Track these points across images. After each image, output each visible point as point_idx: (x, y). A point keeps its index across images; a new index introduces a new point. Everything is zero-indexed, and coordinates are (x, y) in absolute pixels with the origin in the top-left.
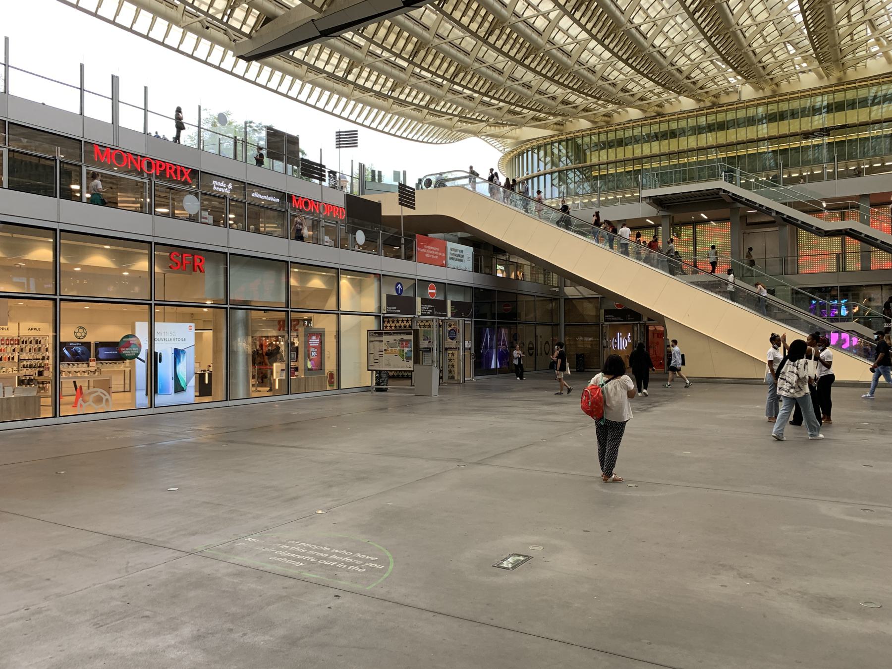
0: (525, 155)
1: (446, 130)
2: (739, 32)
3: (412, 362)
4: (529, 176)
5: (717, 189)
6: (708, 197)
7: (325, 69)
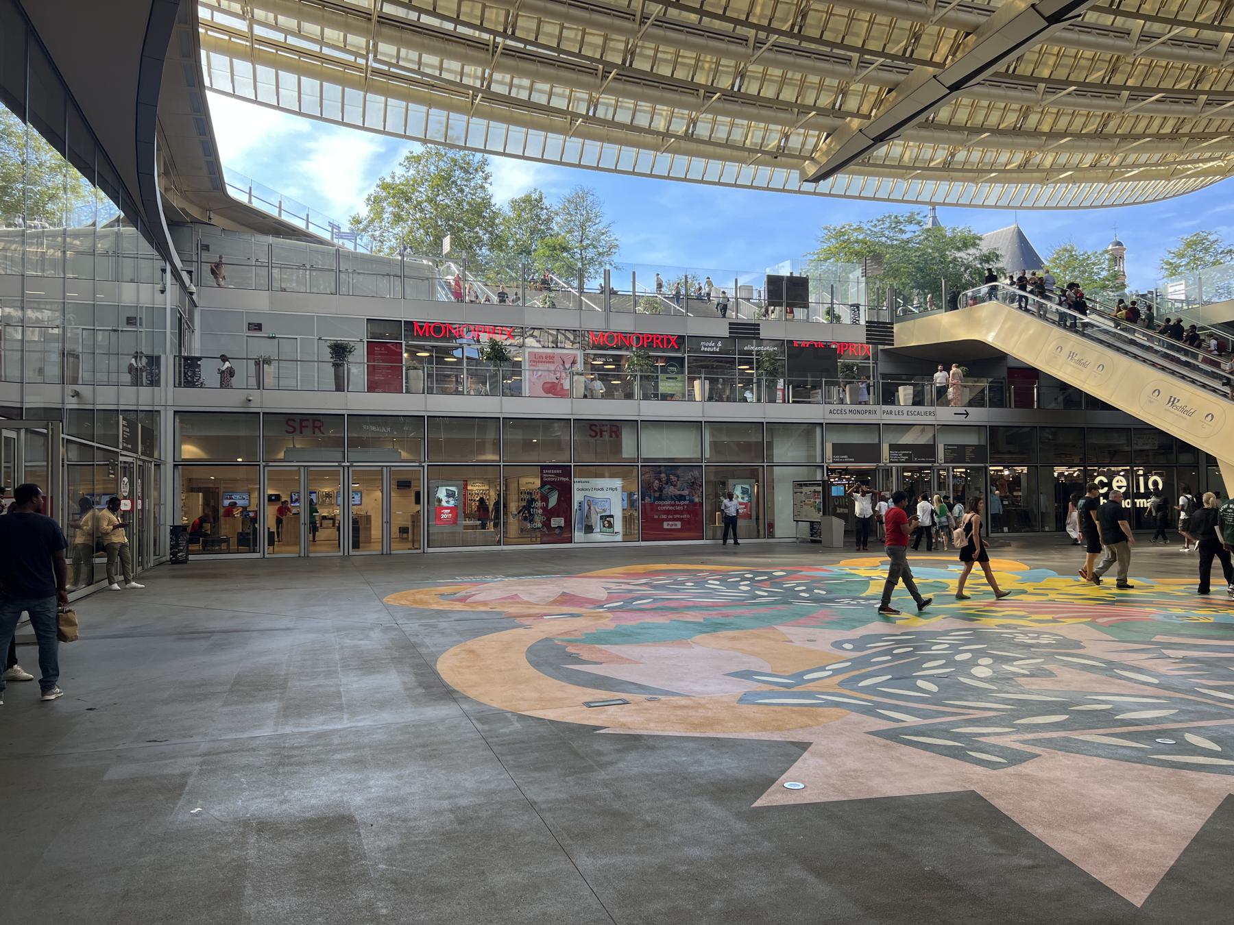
1: (1131, 183)
3: (821, 513)
7: (616, 119)
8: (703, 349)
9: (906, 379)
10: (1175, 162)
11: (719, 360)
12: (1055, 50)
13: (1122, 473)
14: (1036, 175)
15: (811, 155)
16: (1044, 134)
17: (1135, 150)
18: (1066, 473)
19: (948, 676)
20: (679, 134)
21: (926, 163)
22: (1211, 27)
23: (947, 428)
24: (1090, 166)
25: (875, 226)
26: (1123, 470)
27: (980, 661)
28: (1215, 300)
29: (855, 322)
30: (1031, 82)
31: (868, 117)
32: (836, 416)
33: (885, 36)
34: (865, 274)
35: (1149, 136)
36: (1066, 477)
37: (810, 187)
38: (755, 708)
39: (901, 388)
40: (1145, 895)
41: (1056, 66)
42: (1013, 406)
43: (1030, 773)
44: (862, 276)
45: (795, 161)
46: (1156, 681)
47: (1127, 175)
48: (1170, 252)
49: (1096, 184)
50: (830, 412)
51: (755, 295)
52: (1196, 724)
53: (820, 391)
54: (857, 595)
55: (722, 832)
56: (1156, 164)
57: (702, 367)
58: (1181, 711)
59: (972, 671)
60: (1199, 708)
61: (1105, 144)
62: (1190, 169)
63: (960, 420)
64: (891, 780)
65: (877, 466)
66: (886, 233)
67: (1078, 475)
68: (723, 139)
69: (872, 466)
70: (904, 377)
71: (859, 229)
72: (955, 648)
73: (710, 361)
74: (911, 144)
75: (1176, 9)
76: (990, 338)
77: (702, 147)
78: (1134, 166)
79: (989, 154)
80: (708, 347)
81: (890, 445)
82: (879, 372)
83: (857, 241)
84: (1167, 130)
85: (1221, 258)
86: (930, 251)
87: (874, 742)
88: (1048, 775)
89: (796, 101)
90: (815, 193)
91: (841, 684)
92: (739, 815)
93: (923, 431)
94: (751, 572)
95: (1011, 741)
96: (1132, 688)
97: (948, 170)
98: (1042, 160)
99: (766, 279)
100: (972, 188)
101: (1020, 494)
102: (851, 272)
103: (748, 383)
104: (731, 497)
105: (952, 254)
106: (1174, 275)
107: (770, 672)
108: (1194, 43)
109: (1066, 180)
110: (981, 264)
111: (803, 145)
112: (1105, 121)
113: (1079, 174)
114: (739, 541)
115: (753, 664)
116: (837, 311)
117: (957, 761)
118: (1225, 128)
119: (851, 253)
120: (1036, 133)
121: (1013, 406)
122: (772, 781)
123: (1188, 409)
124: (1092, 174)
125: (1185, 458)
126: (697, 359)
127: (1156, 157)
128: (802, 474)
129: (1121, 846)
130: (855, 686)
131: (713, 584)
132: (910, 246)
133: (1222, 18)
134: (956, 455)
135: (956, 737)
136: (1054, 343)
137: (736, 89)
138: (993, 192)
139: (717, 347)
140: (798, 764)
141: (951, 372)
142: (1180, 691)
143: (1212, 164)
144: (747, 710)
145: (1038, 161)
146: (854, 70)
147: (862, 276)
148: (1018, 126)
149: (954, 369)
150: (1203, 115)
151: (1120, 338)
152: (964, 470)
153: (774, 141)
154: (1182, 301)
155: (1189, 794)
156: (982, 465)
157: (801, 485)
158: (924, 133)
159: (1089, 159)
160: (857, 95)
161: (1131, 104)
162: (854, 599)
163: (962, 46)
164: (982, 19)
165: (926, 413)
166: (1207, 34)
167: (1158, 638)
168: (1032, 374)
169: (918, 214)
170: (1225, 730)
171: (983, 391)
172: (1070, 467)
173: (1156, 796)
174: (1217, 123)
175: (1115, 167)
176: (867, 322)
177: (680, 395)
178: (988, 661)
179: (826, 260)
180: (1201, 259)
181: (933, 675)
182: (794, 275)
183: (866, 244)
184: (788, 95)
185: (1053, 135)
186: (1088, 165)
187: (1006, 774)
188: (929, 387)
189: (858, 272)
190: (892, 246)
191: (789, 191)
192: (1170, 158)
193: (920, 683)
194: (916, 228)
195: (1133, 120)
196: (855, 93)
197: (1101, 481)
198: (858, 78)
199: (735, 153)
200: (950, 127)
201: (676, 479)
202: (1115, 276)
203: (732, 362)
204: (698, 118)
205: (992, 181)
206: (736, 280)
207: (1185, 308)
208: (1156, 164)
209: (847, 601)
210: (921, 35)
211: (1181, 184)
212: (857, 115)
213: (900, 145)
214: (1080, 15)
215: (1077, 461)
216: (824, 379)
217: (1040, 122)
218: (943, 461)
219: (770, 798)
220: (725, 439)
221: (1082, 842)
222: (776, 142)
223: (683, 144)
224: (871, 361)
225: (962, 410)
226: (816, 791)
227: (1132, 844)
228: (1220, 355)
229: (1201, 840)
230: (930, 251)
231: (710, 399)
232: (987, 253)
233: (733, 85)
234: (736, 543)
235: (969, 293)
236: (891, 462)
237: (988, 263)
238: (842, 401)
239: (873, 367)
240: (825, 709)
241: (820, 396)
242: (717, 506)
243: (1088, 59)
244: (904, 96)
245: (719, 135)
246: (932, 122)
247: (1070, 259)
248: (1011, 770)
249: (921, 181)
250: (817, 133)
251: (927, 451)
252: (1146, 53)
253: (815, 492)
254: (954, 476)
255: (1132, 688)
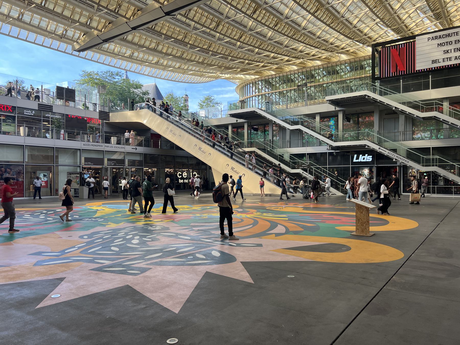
0: (249, 85)
2: (388, 5)
3: (79, 185)
4: (248, 97)
5: (364, 95)
6: (355, 101)
8: (25, 113)
9: (114, 134)
10: (202, 72)
11: (33, 119)
12: (168, 25)
13: (186, 171)
14: (161, 67)
15: (77, 40)
16: (164, 53)
17: (192, 65)
18: (169, 171)
19: (123, 244)
20: (15, 17)
21: (123, 54)
22: (213, 30)
23: (129, 153)
24: (178, 67)
25: (104, 74)
26: (186, 170)
27: (135, 238)
28: (213, 118)
29: (95, 110)
30: (160, 34)
31: (101, 31)
32: (86, 147)
33: (108, 2)
34: (99, 92)
35: (195, 61)
36: (169, 172)
37: (75, 53)
38: (41, 267)
39: (112, 138)
40: (179, 309)
41: (168, 31)
42: (152, 147)
43: (148, 275)
44: (98, 93)
45: (70, 41)
46: (189, 238)
47: (189, 73)
48: (201, 101)
49: (176, 73)
50: (84, 145)
51: (52, 94)
52: (199, 251)
53: (79, 136)
54: (91, 217)
55: (20, 322)
56: (197, 71)
57: (25, 121)
58: (196, 247)
59: (132, 242)
60: (201, 245)
61: (182, 61)
62: (207, 75)
63: (134, 151)
64: (97, 286)
65: (102, 167)
66: (108, 77)
67: (173, 172)
68: (28, 21)
69: (100, 167)
70: (114, 133)
71: (97, 74)
72: (127, 234)
73: (28, 119)
74: (118, 46)
75: (204, 22)
76: (145, 122)
77: (26, 26)
78: (191, 70)
79: (146, 56)
80: (27, 113)
81: (108, 159)
82: (104, 131)
83: (96, 79)
84: (200, 61)
85: (215, 105)
86: (125, 87)
87: (92, 273)
88: (154, 275)
89: (71, 17)
90: (78, 56)
91: (81, 252)
92: (28, 313)
93: (120, 154)
94: (46, 210)
95: (143, 265)
96: (182, 241)
97: (131, 58)
98: (163, 62)
99: (56, 88)
100: (140, 67)
101: (154, 178)
102: (94, 90)
103: (47, 130)
104: (38, 178)
105: (132, 90)
106: (202, 108)
107: (50, 251)
108: (209, 34)
109: (170, 71)
110: (142, 95)
111: (74, 36)
112: (183, 53)
113: (174, 70)
114: (42, 197)
115: (42, 248)
116: (87, 105)
117: (123, 275)
118: (216, 64)
119: (94, 83)
120: (161, 52)
121: (152, 147)
122: (46, 296)
123: (204, 151)
124: (178, 70)
125: (203, 167)
126: (23, 118)
127: (197, 69)
128: (71, 169)
129: (174, 294)
130: (87, 252)
131: (27, 216)
132: (117, 84)
133: (216, 28)
134: (132, 163)
135: (123, 266)
136: (166, 126)
137: (43, 5)
138: (147, 70)
139: (32, 113)
140: (59, 287)
141: (131, 133)
142: (196, 241)
143: (213, 74)
144: (38, 268)
145: (162, 62)
146: (95, 11)
147: (98, 93)
148: (156, 48)
149: (132, 132)
150: (211, 58)
151: (193, 131)
152: (135, 169)
153: (60, 31)
154: (204, 117)
155: (196, 273)
156: (141, 167)
157: (71, 174)
158: (122, 42)
159: (178, 65)
160: (96, 21)
161: (190, 50)
162: (90, 218)
163: (136, 14)
164: (144, 7)
165: (121, 148)
166: (212, 32)
167: (192, 224)
168: (158, 136)
169: (120, 73)
170: (207, 251)
171: (142, 141)
172: (170, 169)
173: (186, 276)
174: (214, 62)
175: (186, 70)
176: (99, 111)
177: (13, 133)
178: (138, 237)
179: (83, 84)
180: (209, 104)
181: (117, 245)
182: (69, 88)
183: (100, 80)
184: (67, 13)
185: (167, 54)
186: (177, 67)
187: (140, 277)
188: (123, 138)
189: (96, 91)
190: (110, 83)
191: (67, 53)
192: (201, 70)
193: (112, 248)
194: (119, 78)
195: (191, 55)
196: (96, 20)
197: (179, 174)
198: (97, 15)
199: (42, 32)
200: (132, 43)
201: (10, 170)
202: (185, 106)
203: (40, 120)
204: (24, 13)
205: (146, 66)
206: (42, 86)
207: (205, 119)
208: (197, 71)
209: (87, 219)
210: (121, 5)
211: (204, 79)
212: (96, 29)
213: (113, 45)
214: (175, 15)
215: (172, 167)
216: (81, 132)
217: (162, 49)
218: (127, 166)
219: (44, 303)
220: (36, 153)
221: (162, 295)
222: (61, 32)
223: (17, 22)
224: (101, 126)
225: (134, 147)
226: (65, 297)
227: (177, 293)
228: (221, 140)
229: (197, 287)
230: (125, 87)
231: (28, 135)
232: (145, 91)
233: (41, 3)
234: (40, 198)
235: (139, 105)
236: (108, 165)
237: (145, 95)
238: (89, 141)
239: (102, 129)
240: (74, 263)
241: (79, 138)
242: (31, 183)
243: (178, 31)
244: (115, 27)
245: (34, 22)
246: (126, 39)
247: (172, 97)
248: (141, 275)
249: (121, 61)
250: (80, 32)
251: (122, 162)
252: (195, 34)
253: (76, 176)
254: (131, 171)
255: (182, 241)
